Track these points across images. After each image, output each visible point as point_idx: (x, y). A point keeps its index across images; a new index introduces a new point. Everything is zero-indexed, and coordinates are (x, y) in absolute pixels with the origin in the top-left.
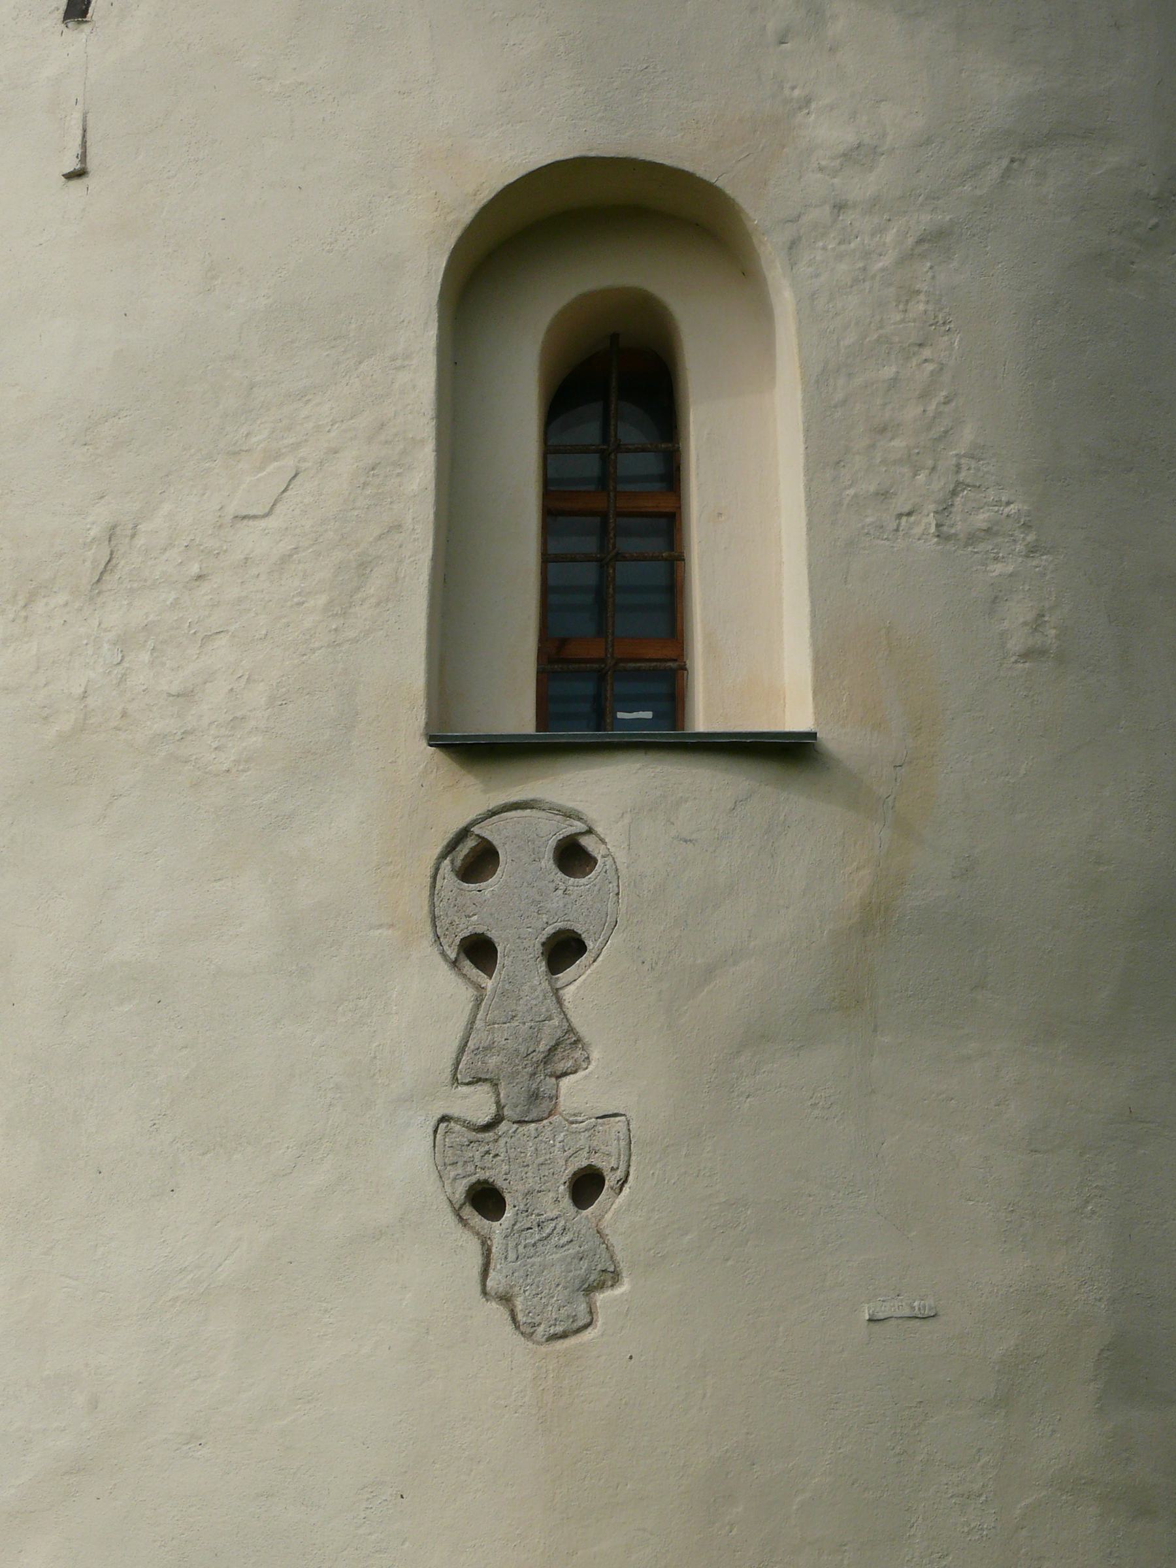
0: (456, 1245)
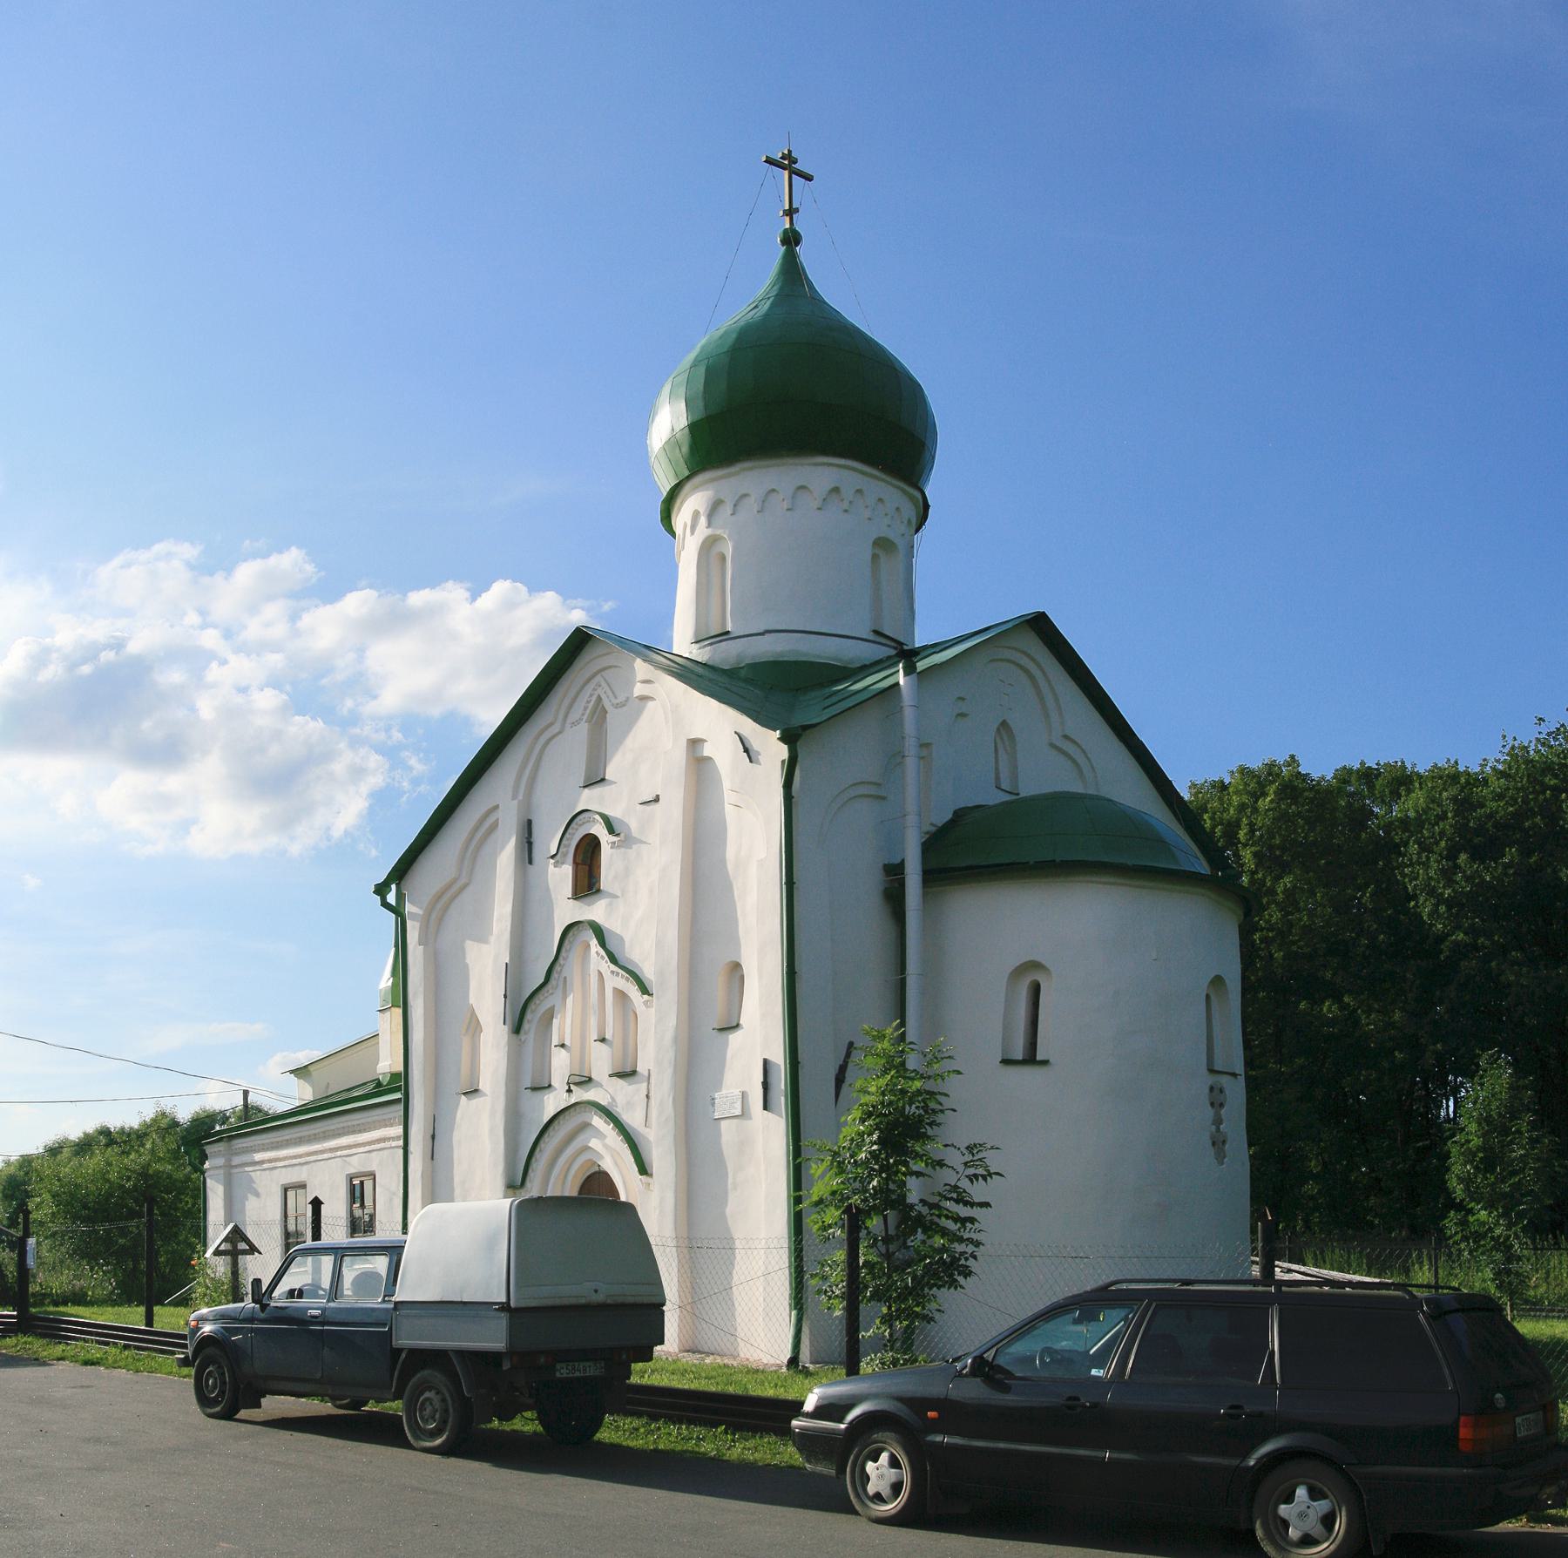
0: (1211, 1151)
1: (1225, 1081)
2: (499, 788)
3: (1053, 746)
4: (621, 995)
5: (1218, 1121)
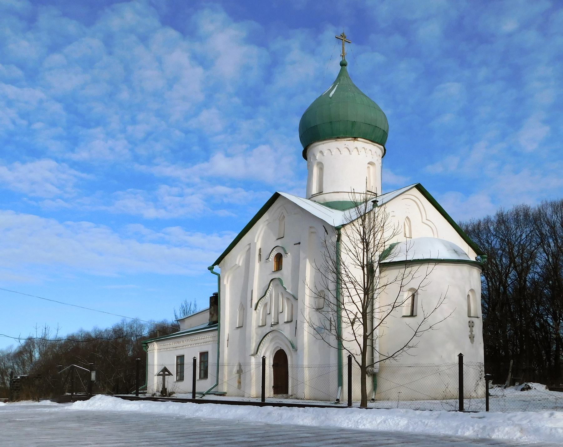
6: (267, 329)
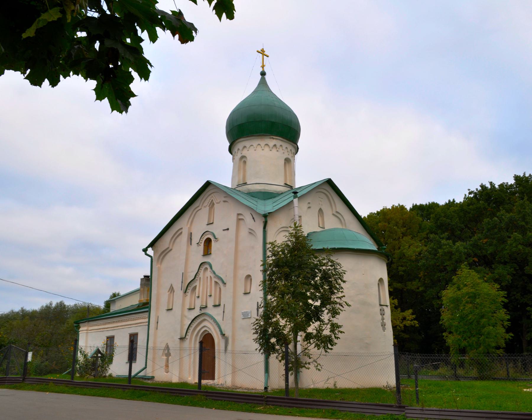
1: (384, 307)
2: (183, 223)
3: (333, 214)
4: (216, 282)
5: (383, 319)
6: (197, 312)
